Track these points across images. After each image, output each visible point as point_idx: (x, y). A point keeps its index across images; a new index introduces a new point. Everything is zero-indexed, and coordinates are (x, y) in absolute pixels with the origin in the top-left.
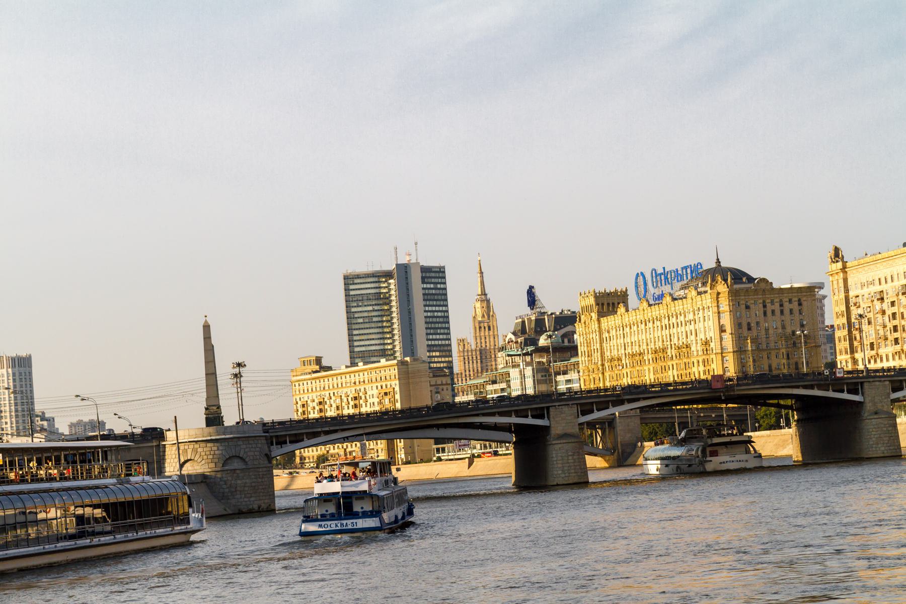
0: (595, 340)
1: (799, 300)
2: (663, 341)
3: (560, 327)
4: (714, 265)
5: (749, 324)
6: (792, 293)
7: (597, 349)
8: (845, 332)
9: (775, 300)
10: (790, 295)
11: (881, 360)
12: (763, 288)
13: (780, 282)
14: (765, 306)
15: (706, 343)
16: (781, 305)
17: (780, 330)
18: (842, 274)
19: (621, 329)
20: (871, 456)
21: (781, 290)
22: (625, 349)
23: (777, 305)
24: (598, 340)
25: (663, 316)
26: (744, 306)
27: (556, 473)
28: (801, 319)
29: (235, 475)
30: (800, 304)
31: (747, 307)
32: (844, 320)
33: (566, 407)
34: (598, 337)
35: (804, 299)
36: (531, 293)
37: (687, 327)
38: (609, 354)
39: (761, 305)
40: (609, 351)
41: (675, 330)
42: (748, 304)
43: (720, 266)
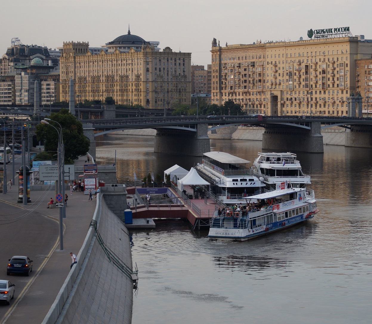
0: (71, 67)
2: (112, 72)
3: (33, 53)
5: (160, 68)
6: (181, 55)
7: (72, 71)
8: (218, 80)
10: (179, 56)
11: (236, 95)
12: (168, 52)
13: (146, 40)
15: (138, 76)
16: (175, 61)
17: (174, 73)
18: (218, 53)
19: (88, 63)
20: (312, 152)
21: (176, 54)
22: (89, 73)
23: (182, 60)
24: (73, 67)
25: (113, 59)
26: (159, 59)
27: (199, 151)
28: (184, 68)
30: (184, 61)
32: (218, 74)
33: (204, 124)
34: (73, 65)
35: (186, 59)
37: (127, 67)
38: (79, 74)
40: (79, 73)
41: (120, 67)
43: (130, 34)
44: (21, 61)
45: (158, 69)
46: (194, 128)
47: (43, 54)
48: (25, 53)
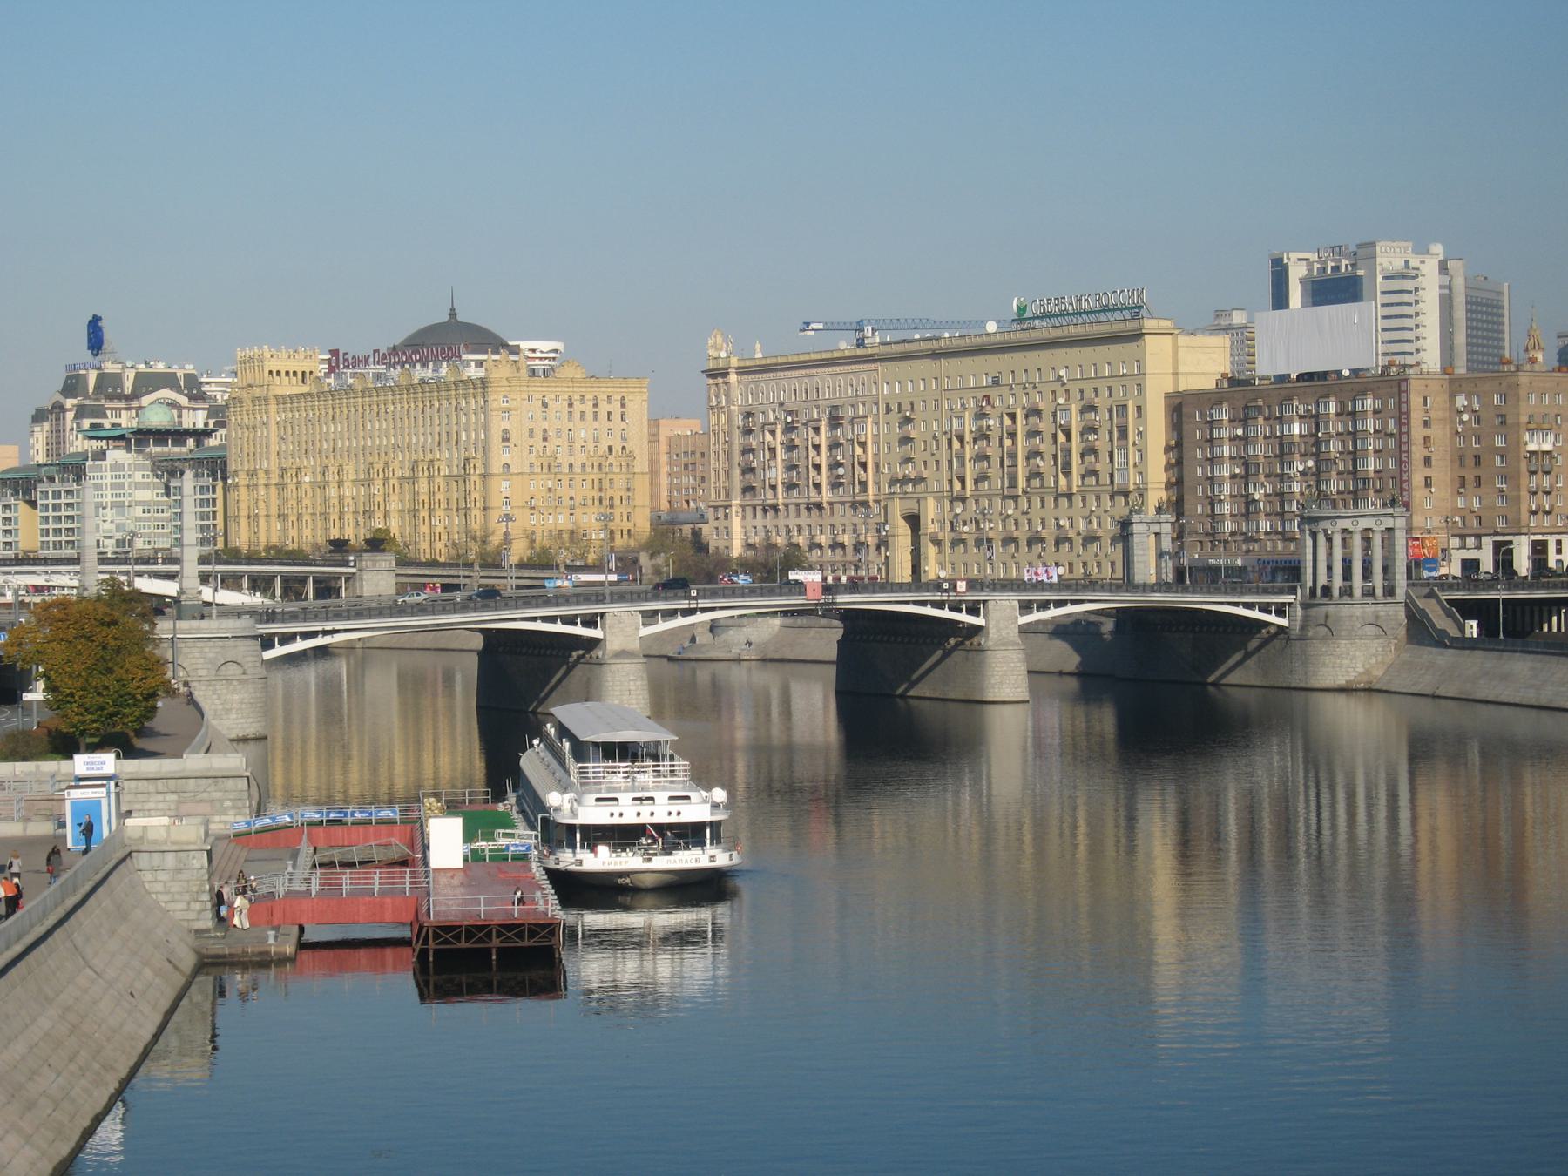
1: (623, 398)
3: (147, 389)
4: (445, 318)
9: (587, 397)
14: (571, 405)
16: (595, 405)
29: (231, 687)
30: (623, 405)
31: (545, 405)
35: (630, 398)
36: (95, 325)
39: (566, 403)
42: (546, 400)
44: (109, 413)
45: (539, 434)
46: (596, 627)
47: (179, 390)
48: (122, 389)
